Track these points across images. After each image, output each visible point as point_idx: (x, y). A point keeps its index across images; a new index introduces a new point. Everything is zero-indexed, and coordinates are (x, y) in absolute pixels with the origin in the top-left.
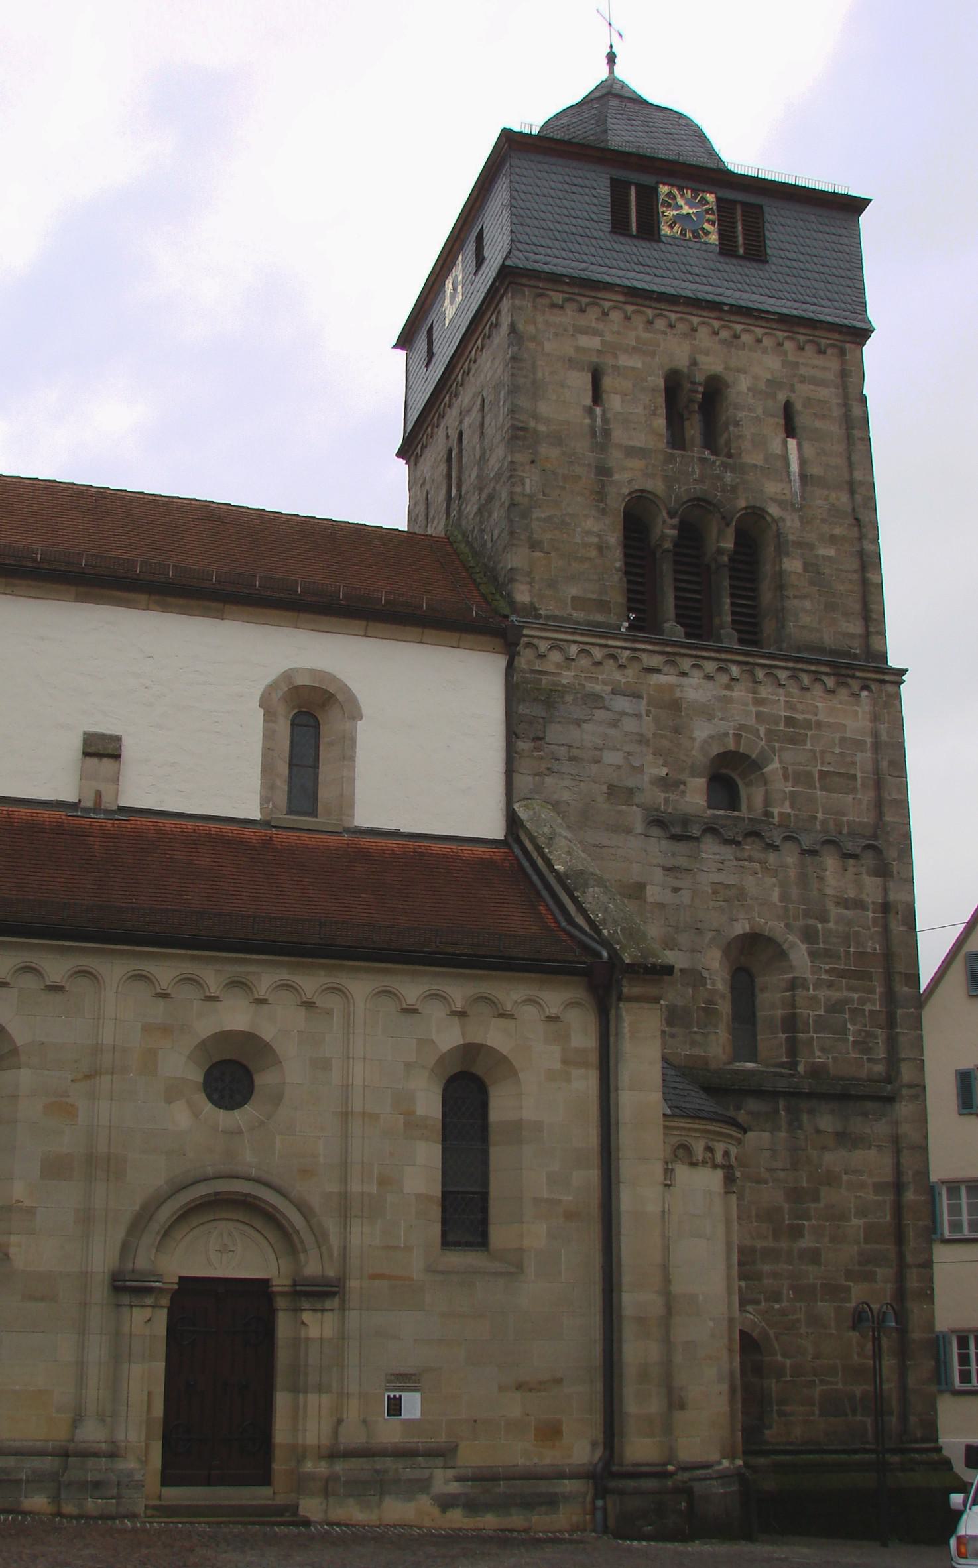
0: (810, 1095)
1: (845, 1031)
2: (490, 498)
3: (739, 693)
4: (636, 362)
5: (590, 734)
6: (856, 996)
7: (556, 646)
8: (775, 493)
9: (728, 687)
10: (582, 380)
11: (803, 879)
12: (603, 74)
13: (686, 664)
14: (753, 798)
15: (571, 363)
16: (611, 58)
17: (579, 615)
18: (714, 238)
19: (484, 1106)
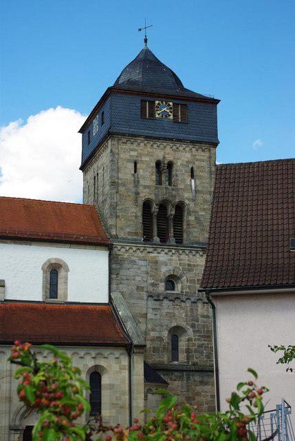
0: (193, 371)
1: (202, 353)
2: (105, 200)
3: (175, 257)
4: (147, 159)
5: (131, 272)
6: (206, 343)
7: (123, 247)
8: (187, 196)
9: (171, 256)
10: (132, 165)
11: (192, 309)
12: (142, 46)
13: (159, 250)
14: (179, 287)
15: (128, 161)
16: (146, 41)
17: (130, 237)
18: (171, 117)
19: (100, 380)
